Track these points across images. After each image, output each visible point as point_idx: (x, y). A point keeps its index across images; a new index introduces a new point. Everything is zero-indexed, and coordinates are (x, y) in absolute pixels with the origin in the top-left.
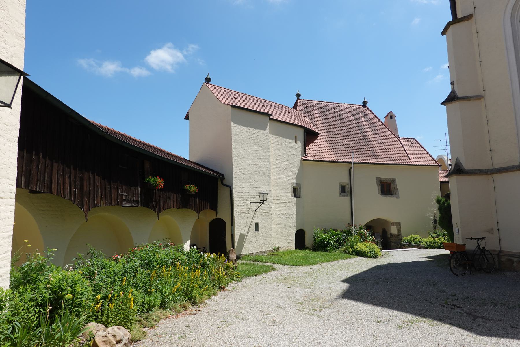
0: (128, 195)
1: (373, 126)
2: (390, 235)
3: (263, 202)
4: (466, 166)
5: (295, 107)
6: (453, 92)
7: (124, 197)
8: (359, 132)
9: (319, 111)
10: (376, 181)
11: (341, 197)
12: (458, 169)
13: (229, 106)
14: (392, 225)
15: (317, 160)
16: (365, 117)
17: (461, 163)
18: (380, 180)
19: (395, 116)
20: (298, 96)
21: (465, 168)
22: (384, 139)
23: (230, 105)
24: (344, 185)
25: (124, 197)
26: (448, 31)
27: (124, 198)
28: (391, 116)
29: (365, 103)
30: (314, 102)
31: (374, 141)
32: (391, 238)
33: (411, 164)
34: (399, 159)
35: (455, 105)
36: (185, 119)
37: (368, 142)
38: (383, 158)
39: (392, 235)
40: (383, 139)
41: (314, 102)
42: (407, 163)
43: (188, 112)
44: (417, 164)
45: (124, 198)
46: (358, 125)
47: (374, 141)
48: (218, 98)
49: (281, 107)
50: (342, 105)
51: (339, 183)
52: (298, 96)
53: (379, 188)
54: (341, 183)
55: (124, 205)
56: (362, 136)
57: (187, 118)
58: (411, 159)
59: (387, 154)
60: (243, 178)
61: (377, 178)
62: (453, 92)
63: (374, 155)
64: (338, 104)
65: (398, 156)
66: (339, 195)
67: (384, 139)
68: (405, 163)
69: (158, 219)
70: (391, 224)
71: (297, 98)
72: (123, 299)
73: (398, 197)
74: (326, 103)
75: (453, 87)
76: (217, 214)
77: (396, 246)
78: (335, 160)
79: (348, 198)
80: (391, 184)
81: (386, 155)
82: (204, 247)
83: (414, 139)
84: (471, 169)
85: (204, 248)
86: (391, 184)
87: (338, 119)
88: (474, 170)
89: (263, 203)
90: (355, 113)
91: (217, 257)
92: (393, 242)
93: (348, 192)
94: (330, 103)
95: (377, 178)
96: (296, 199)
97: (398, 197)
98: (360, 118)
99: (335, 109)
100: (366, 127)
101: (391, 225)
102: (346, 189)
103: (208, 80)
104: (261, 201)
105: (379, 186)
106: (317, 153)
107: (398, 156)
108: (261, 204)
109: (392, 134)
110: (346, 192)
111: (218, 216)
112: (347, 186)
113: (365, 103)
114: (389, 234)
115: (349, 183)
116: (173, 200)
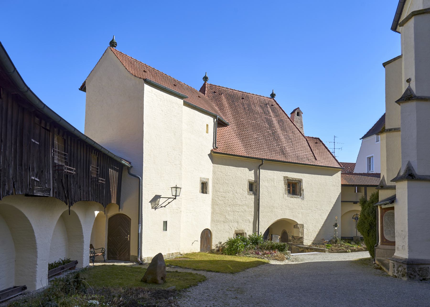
0: (40, 180)
1: (281, 122)
2: (292, 238)
3: (176, 197)
4: (418, 171)
5: (203, 90)
6: (410, 91)
7: (35, 183)
8: (268, 126)
9: (227, 99)
12: (410, 174)
13: (142, 80)
14: (295, 227)
15: (228, 153)
16: (273, 111)
17: (412, 167)
19: (302, 113)
20: (205, 79)
21: (417, 174)
22: (292, 136)
23: (144, 79)
25: (35, 183)
26: (408, 21)
27: (36, 185)
28: (297, 112)
29: (273, 95)
30: (222, 88)
31: (282, 137)
33: (317, 164)
34: (306, 158)
35: (412, 105)
36: (80, 89)
37: (277, 139)
38: (292, 156)
39: (294, 238)
40: (291, 135)
41: (222, 88)
42: (313, 164)
43: (85, 82)
44: (323, 165)
45: (36, 185)
46: (267, 119)
47: (282, 137)
48: (127, 68)
49: (192, 91)
50: (251, 95)
52: (205, 79)
55: (36, 194)
56: (271, 131)
57: (83, 88)
58: (317, 159)
59: (295, 152)
60: (154, 168)
62: (410, 91)
63: (283, 152)
64: (246, 94)
65: (305, 155)
67: (292, 136)
68: (312, 164)
69: (69, 214)
70: (294, 226)
71: (204, 82)
73: (303, 199)
74: (234, 91)
75: (409, 85)
76: (119, 209)
77: (298, 249)
78: (245, 155)
80: (296, 185)
81: (295, 154)
82: (103, 247)
83: (319, 139)
84: (423, 175)
85: (102, 248)
86: (297, 184)
87: (247, 110)
88: (425, 175)
89: (175, 198)
90: (264, 105)
94: (238, 91)
97: (303, 199)
98: (268, 111)
99: (243, 98)
100: (275, 121)
103: (113, 44)
104: (172, 196)
106: (227, 146)
107: (305, 155)
108: (170, 200)
109: (299, 132)
111: (121, 212)
113: (273, 95)
114: (291, 236)
116: (84, 190)
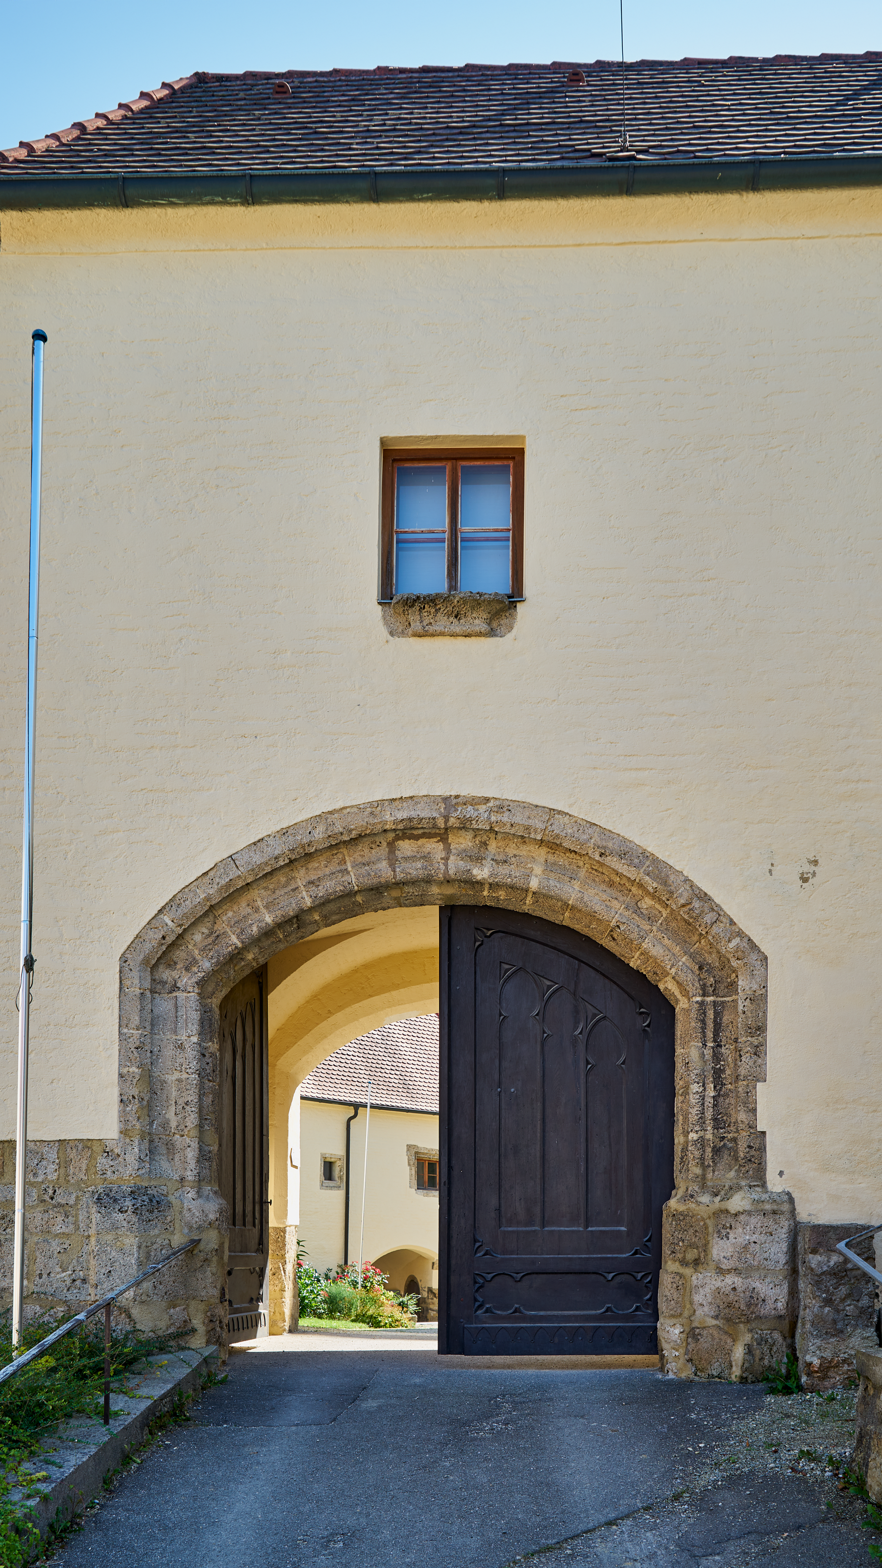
10: (407, 1155)
11: (323, 1191)
18: (416, 1153)
24: (332, 1160)
32: (430, 1300)
51: (322, 1154)
53: (413, 1172)
54: (325, 1154)
61: (409, 1147)
66: (318, 1184)
72: (118, 1295)
79: (342, 1193)
91: (725, 1078)
92: (121, 1293)
93: (341, 1178)
95: (409, 1147)
96: (429, 950)
101: (433, 1268)
102: (336, 1172)
105: (413, 1168)
110: (336, 1178)
112: (338, 1163)
114: (426, 1290)
115: (345, 1154)
